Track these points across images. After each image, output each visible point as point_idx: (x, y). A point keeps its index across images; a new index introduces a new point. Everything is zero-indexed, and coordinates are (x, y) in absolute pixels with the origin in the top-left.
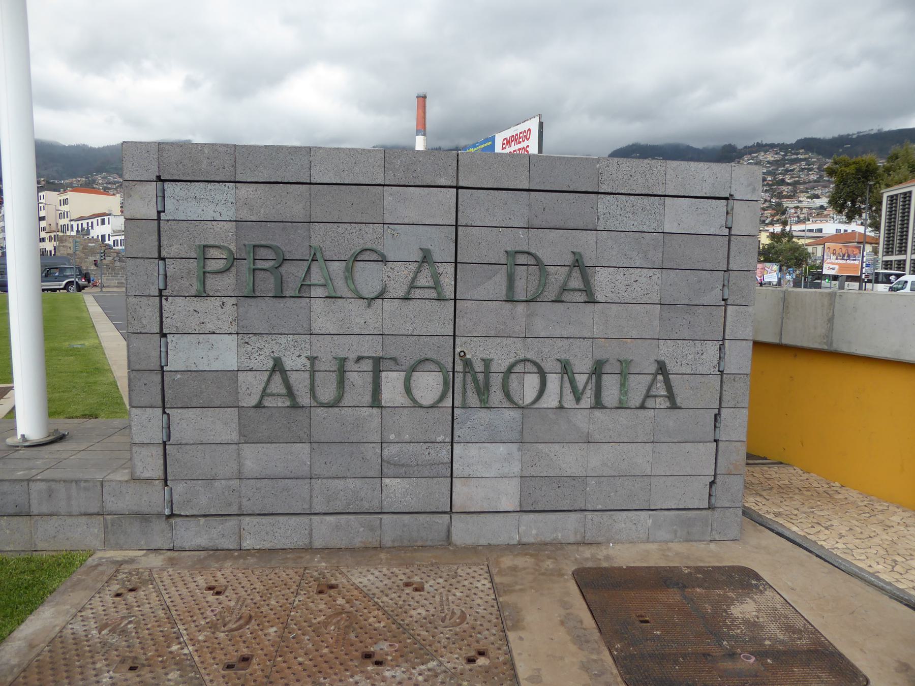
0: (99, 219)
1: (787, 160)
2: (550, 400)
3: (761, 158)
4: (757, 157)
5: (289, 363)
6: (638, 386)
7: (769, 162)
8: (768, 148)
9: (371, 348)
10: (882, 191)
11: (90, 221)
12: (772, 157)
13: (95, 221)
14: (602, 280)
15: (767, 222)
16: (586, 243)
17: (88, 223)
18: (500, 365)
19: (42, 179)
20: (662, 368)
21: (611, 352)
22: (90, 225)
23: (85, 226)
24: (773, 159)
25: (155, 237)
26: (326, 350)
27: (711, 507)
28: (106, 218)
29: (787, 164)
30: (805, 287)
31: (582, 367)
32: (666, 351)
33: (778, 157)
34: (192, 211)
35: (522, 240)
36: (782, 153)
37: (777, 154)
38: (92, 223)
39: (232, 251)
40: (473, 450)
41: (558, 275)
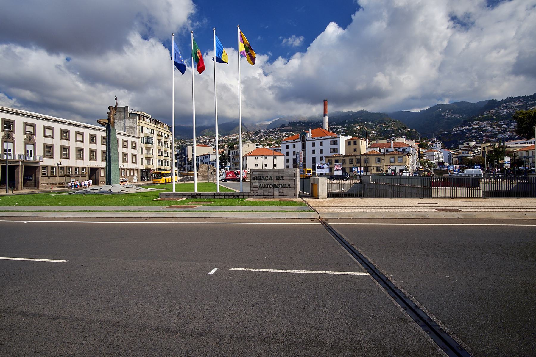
0: (206, 156)
1: (529, 104)
2: (280, 187)
3: (512, 105)
4: (509, 104)
5: (261, 184)
6: (287, 186)
7: (517, 107)
8: (516, 99)
9: (267, 183)
10: (533, 127)
11: (203, 157)
12: (519, 104)
13: (204, 157)
14: (284, 178)
15: (516, 138)
16: (283, 175)
17: (202, 158)
18: (277, 184)
19: (182, 140)
24: (519, 105)
26: (264, 183)
28: (208, 155)
29: (528, 106)
31: (283, 185)
32: (290, 183)
33: (522, 104)
34: (255, 174)
36: (525, 101)
37: (522, 102)
40: (275, 191)
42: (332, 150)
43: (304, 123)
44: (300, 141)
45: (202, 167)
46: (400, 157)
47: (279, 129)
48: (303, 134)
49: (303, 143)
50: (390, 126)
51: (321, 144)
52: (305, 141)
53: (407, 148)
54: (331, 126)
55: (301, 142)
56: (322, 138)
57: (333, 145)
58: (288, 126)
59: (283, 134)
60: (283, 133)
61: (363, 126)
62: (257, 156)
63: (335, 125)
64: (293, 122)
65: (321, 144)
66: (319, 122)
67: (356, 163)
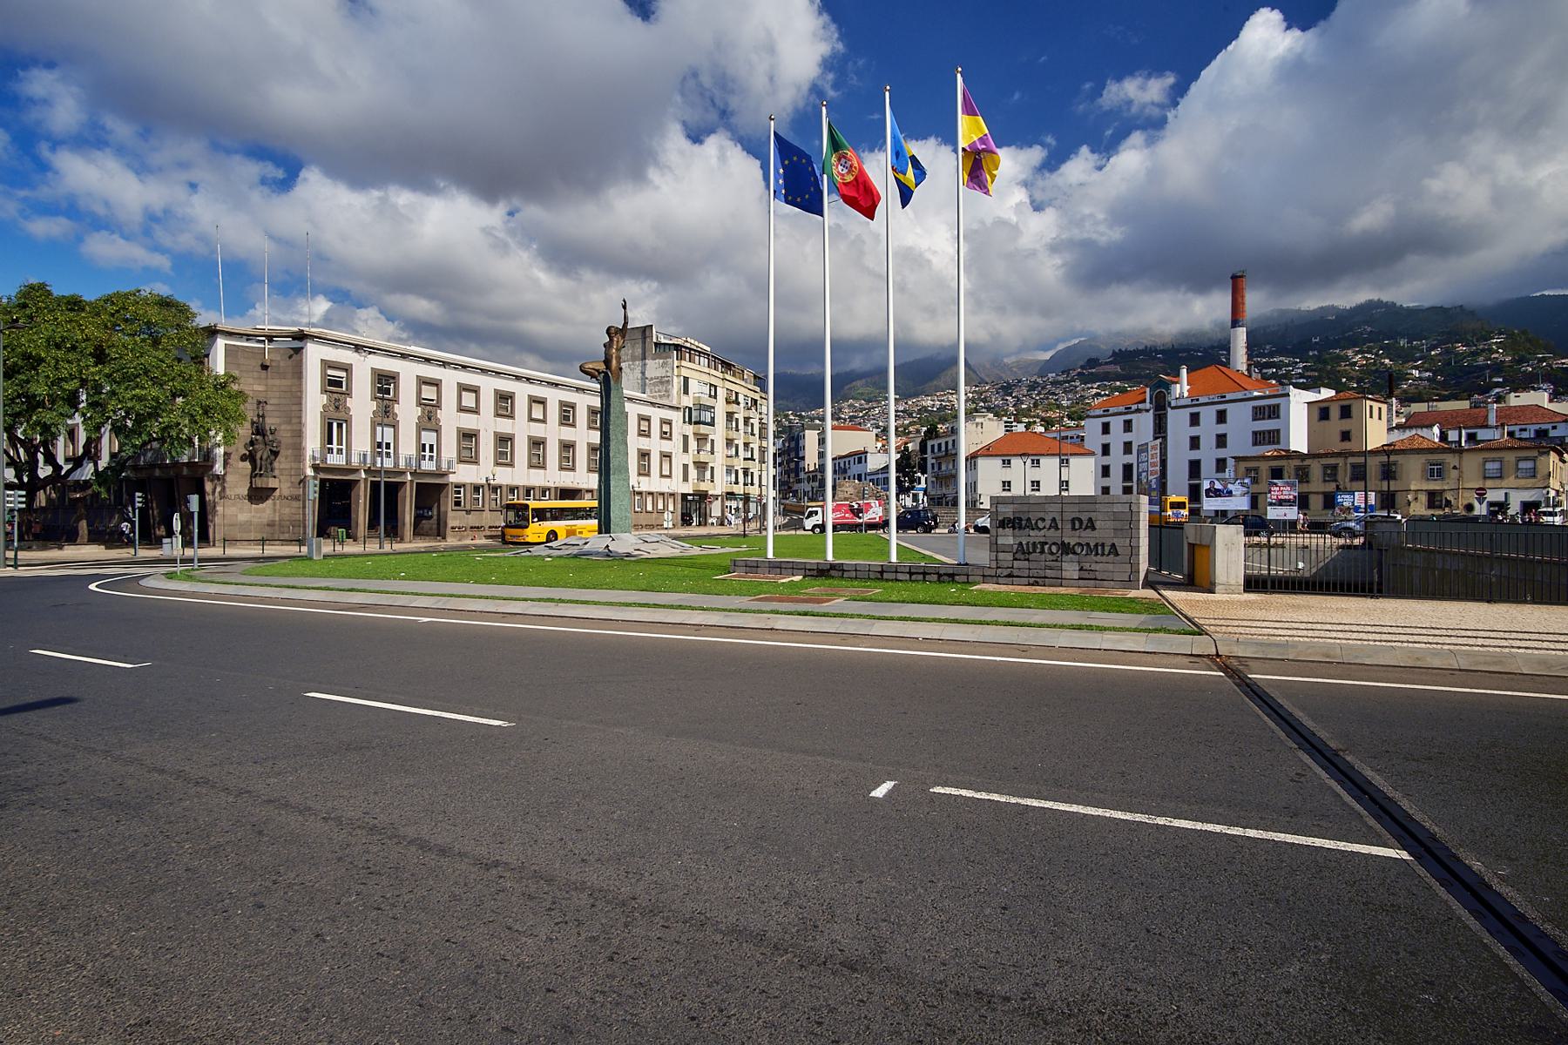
0: (856, 457)
6: (1107, 549)
9: (1042, 540)
11: (847, 460)
13: (852, 459)
14: (1097, 524)
16: (1093, 515)
18: (1072, 544)
19: (790, 412)
20: (1114, 544)
21: (1100, 542)
22: (847, 463)
23: (842, 465)
25: (703, 374)
26: (1032, 540)
27: (1130, 581)
28: (863, 456)
30: (418, 532)
31: (1092, 545)
32: (1115, 541)
34: (1004, 510)
35: (1077, 515)
38: (849, 461)
39: (931, 379)
41: (1085, 523)
42: (1259, 438)
43: (1161, 352)
44: (1148, 407)
45: (846, 490)
46: (1526, 459)
47: (1079, 374)
48: (1159, 387)
49: (1159, 415)
50: (1483, 350)
51: (1221, 417)
52: (1165, 409)
53: (1554, 428)
54: (1255, 359)
55: (1152, 411)
56: (1225, 397)
57: (1264, 419)
58: (1106, 363)
59: (1092, 388)
60: (1090, 386)
61: (1377, 355)
62: (1038, 458)
63: (1271, 355)
64: (1123, 350)
65: (1221, 417)
66: (1212, 347)
67: (1347, 480)
